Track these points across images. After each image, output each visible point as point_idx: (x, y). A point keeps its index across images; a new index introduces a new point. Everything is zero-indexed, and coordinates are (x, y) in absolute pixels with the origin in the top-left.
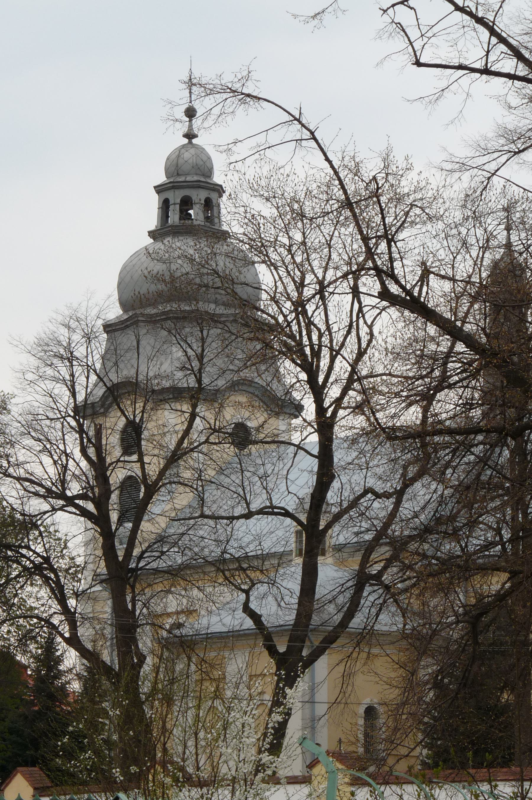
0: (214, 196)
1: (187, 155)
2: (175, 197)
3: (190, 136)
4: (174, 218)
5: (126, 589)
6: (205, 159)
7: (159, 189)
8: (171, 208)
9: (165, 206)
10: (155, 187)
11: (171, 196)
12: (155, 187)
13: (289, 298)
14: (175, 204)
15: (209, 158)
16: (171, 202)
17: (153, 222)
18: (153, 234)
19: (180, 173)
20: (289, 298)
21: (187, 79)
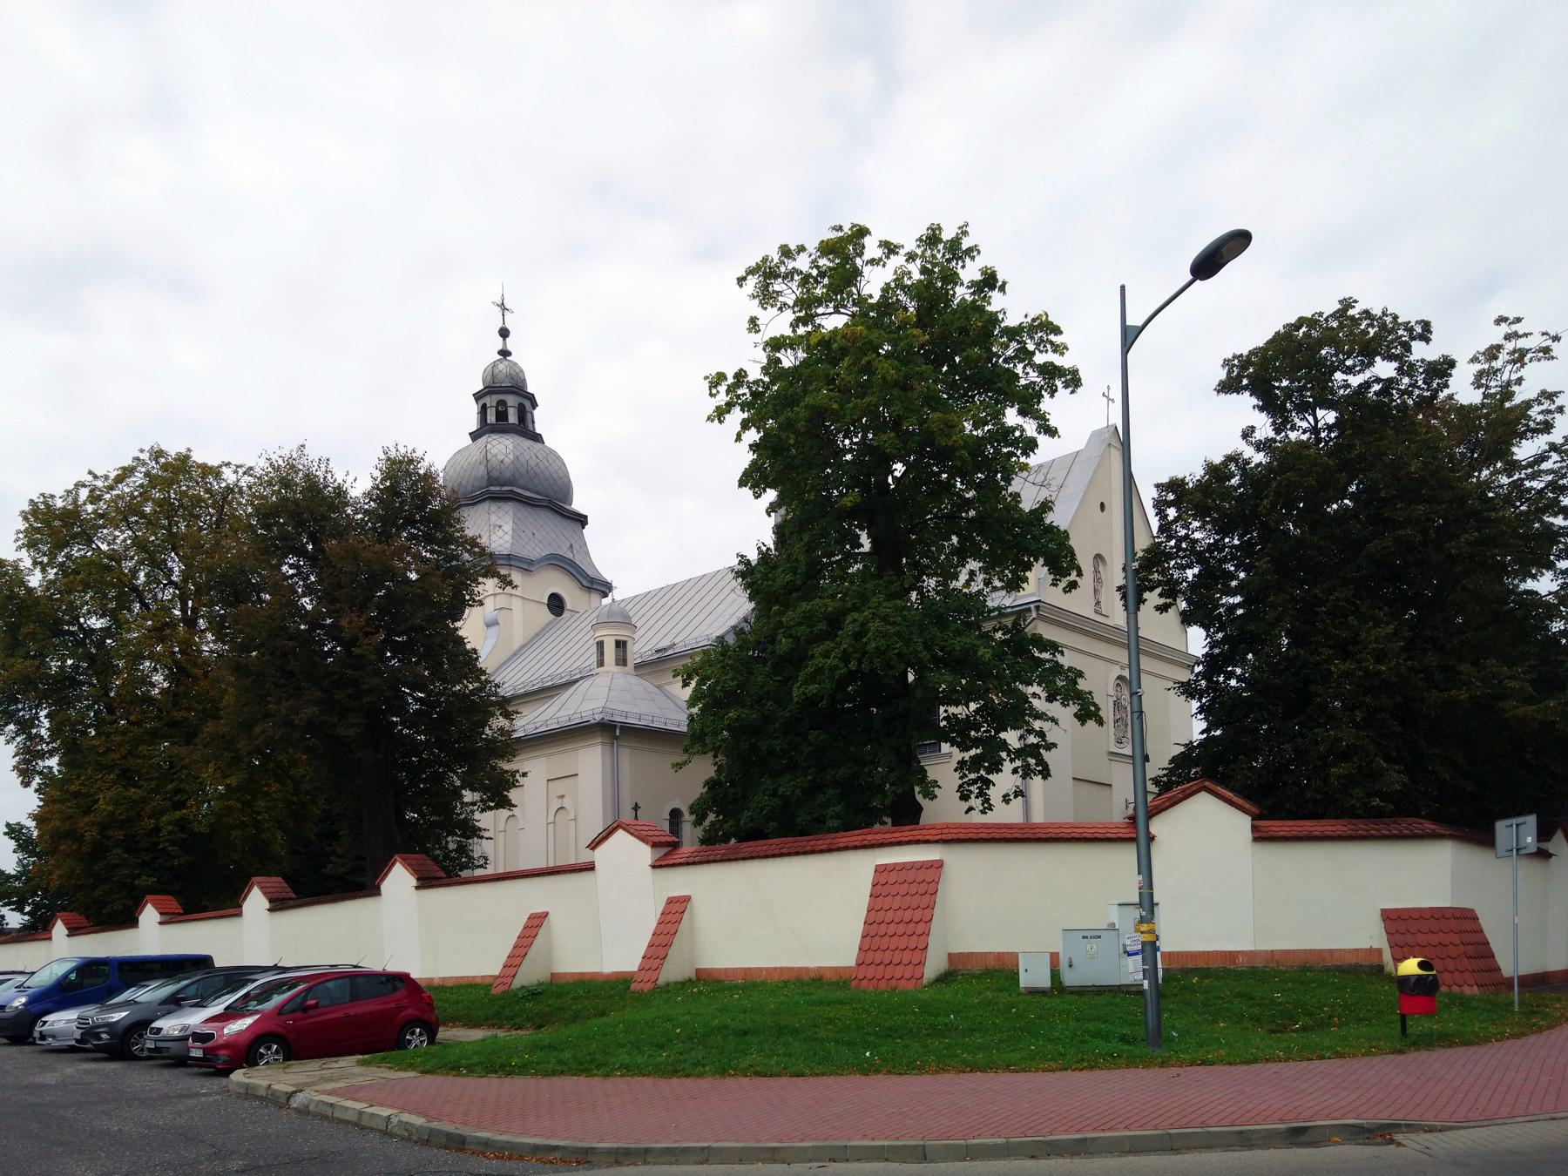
0: (527, 404)
1: (501, 367)
2: (491, 401)
3: (505, 353)
4: (491, 418)
5: (1534, 593)
6: (518, 371)
7: (478, 396)
8: (488, 410)
9: (483, 411)
10: (470, 434)
11: (491, 401)
12: (470, 434)
13: (23, 662)
14: (491, 407)
15: (522, 371)
16: (488, 406)
17: (474, 425)
18: (475, 436)
19: (496, 381)
20: (23, 662)
21: (500, 303)
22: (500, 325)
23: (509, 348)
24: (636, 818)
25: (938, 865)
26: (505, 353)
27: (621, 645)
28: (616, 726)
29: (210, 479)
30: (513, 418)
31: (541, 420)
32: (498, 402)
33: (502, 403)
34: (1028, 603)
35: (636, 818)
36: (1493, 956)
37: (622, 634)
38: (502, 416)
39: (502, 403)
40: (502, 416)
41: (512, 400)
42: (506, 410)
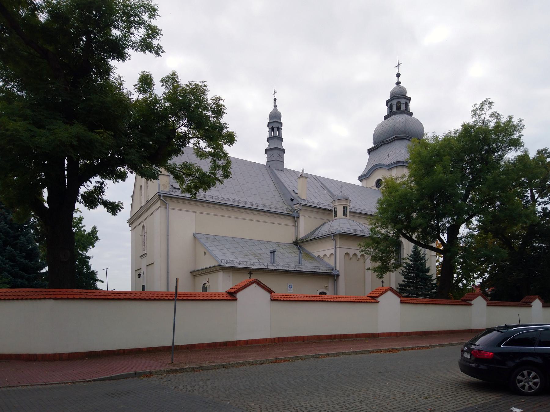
2: (394, 102)
3: (398, 83)
4: (394, 109)
7: (388, 102)
18: (386, 118)
22: (397, 72)
23: (400, 81)
24: (383, 286)
25: (521, 387)
26: (398, 83)
27: (345, 208)
28: (331, 236)
29: (488, 105)
30: (403, 107)
31: (412, 107)
32: (397, 103)
33: (399, 103)
34: (336, 205)
35: (383, 286)
36: (275, 338)
37: (345, 203)
38: (399, 108)
39: (399, 103)
40: (399, 108)
41: (403, 101)
42: (400, 106)
